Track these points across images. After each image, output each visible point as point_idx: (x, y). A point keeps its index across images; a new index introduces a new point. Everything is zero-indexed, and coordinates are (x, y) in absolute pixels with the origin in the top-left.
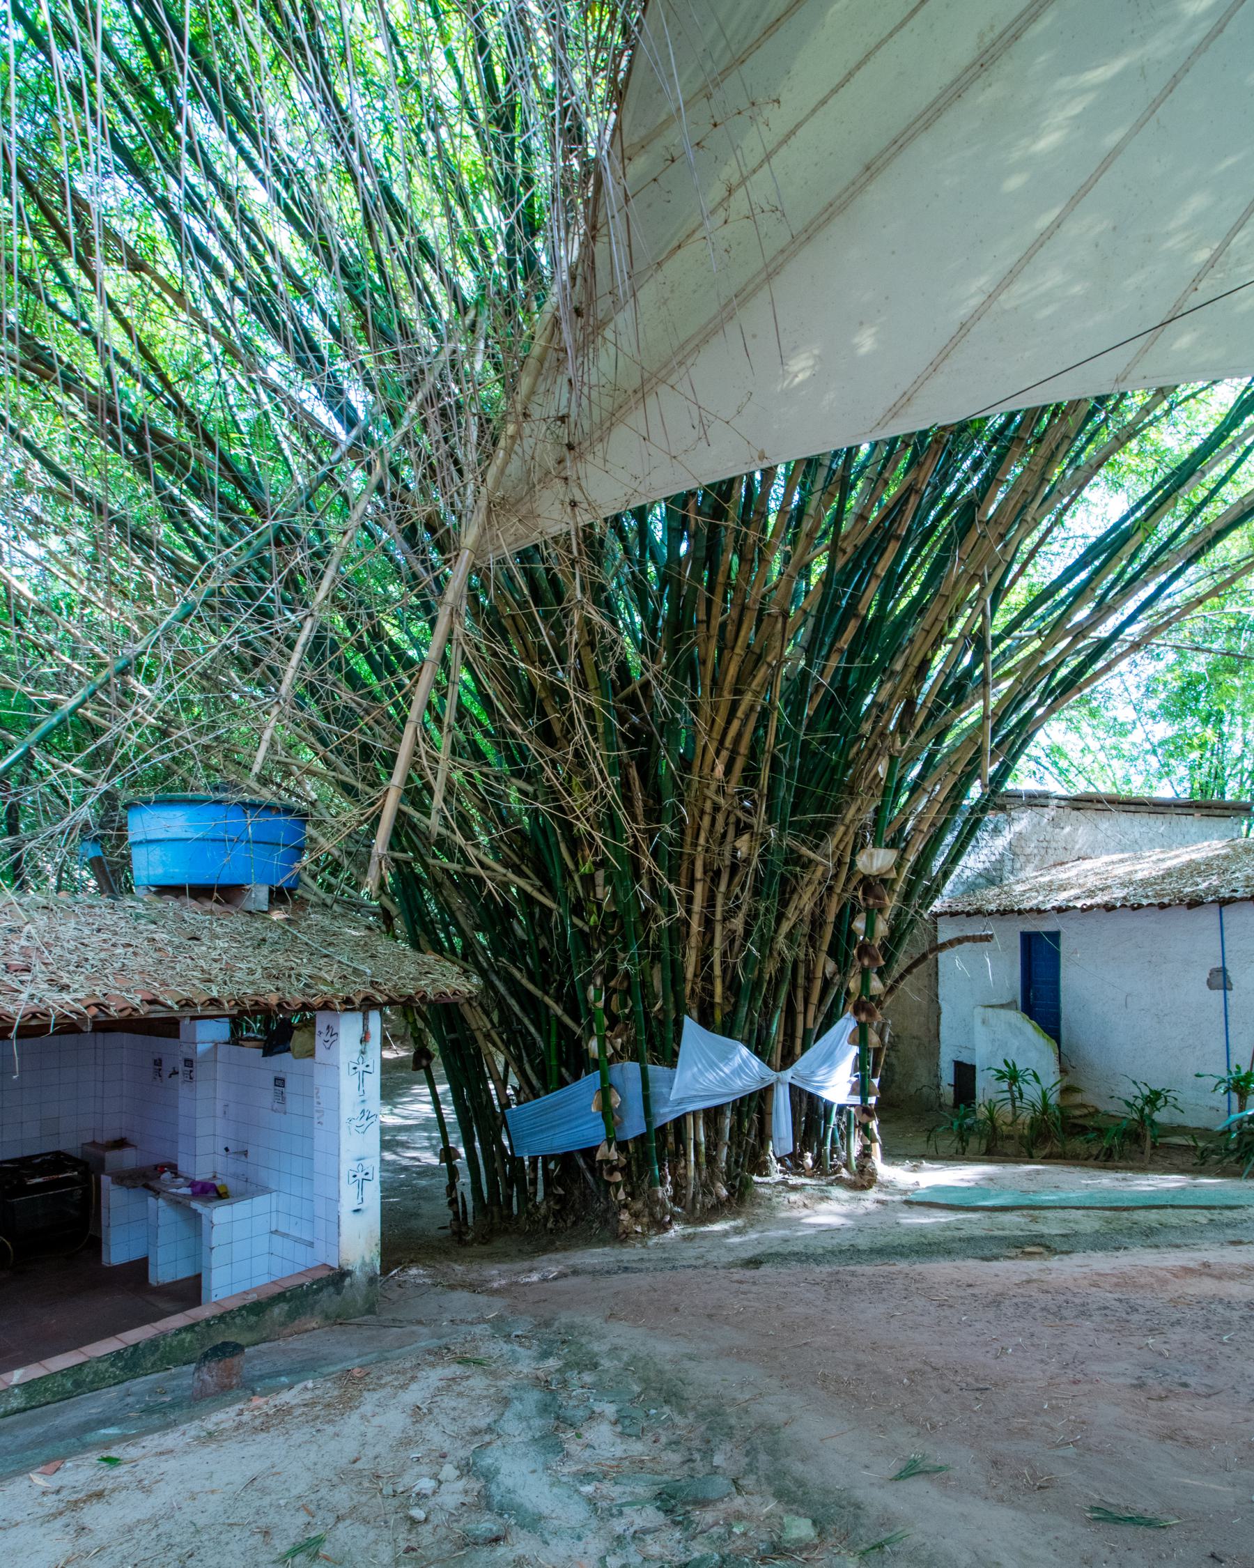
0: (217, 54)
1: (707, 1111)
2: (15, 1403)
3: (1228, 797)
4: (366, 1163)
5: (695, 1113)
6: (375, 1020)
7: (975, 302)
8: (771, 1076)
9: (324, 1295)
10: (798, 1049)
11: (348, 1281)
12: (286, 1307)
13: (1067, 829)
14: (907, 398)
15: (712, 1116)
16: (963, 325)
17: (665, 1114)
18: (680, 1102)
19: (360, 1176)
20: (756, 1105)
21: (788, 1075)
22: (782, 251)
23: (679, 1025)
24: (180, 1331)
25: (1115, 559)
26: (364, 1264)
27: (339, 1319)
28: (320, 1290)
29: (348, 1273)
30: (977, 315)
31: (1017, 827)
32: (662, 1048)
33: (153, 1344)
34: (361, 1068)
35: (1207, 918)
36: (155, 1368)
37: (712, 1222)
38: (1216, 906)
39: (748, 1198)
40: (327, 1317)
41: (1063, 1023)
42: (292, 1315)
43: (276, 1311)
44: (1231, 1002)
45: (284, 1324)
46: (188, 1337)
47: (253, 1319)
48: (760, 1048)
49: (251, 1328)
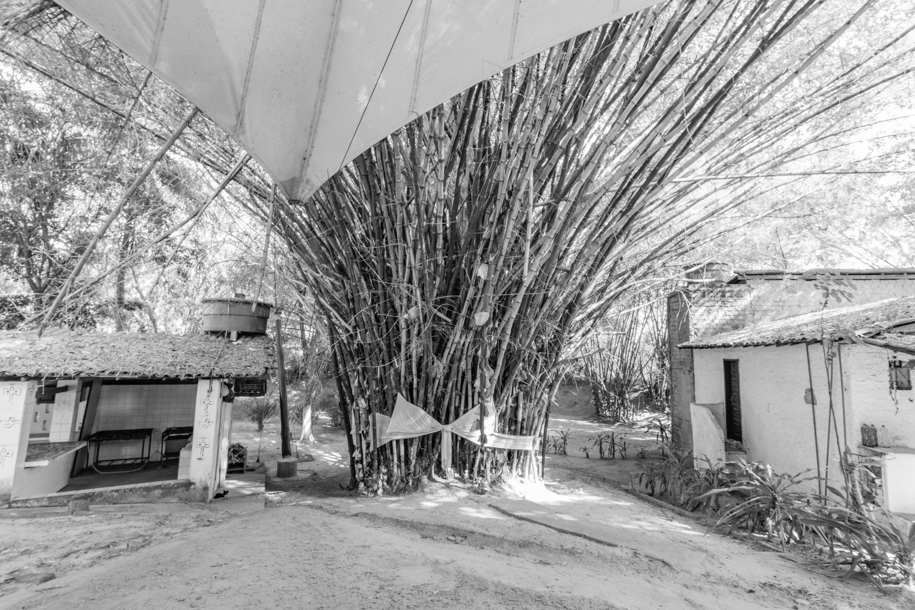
1: (405, 441)
2: (44, 503)
4: (206, 441)
5: (398, 441)
6: (216, 384)
8: (439, 427)
9: (180, 490)
10: (461, 412)
11: (192, 487)
12: (161, 491)
13: (800, 293)
15: (408, 443)
17: (385, 439)
18: (391, 434)
19: (203, 445)
20: (430, 442)
21: (449, 428)
23: (395, 397)
24: (112, 491)
25: (692, 91)
26: (201, 481)
27: (186, 501)
28: (178, 487)
29: (193, 484)
31: (755, 293)
32: (387, 407)
33: (101, 494)
34: (207, 402)
38: (804, 345)
41: (742, 418)
42: (163, 495)
44: (817, 413)
45: (159, 498)
46: (116, 494)
47: (145, 493)
48: (436, 415)
49: (144, 496)
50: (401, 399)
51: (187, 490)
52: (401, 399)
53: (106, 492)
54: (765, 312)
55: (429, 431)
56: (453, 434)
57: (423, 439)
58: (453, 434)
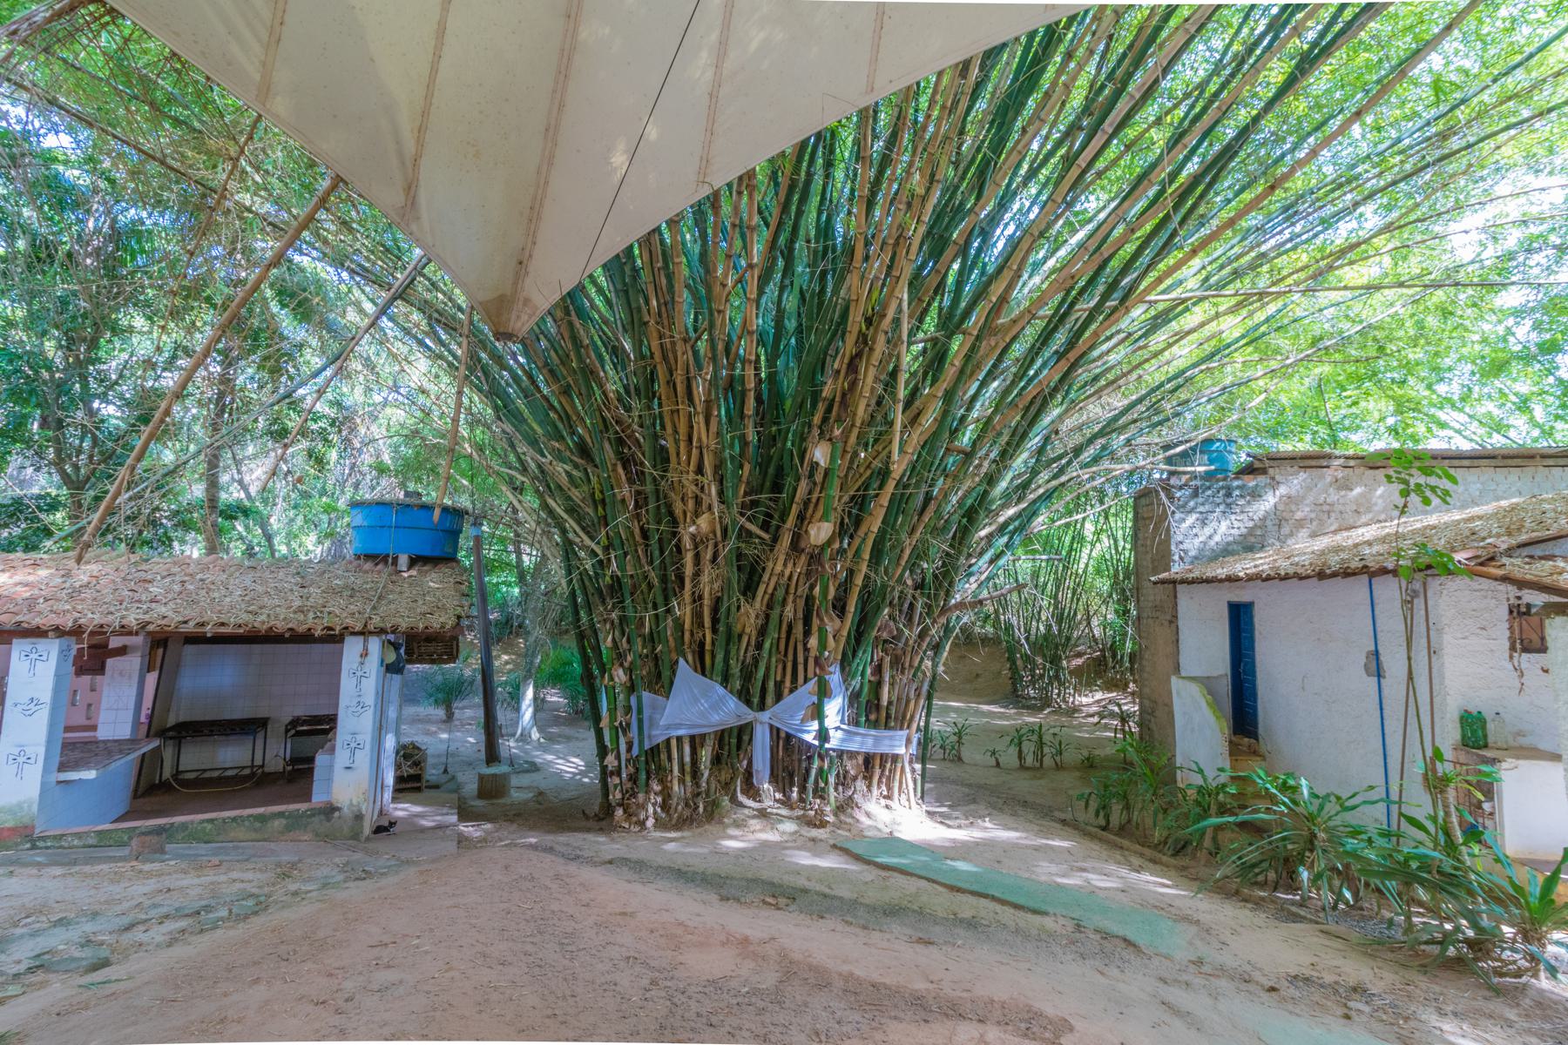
0: (1156, 188)
2: (90, 841)
3: (385, 319)
5: (679, 739)
6: (375, 644)
7: (709, 74)
8: (749, 715)
9: (316, 819)
11: (337, 814)
12: (284, 821)
14: (706, 161)
16: (711, 95)
18: (668, 727)
19: (353, 745)
20: (734, 741)
21: (765, 716)
22: (554, 91)
27: (327, 838)
29: (338, 809)
30: (717, 83)
31: (1282, 490)
32: (660, 680)
33: (184, 826)
35: (1359, 586)
36: (184, 841)
37: (832, 869)
38: (1365, 578)
39: (716, 817)
40: (317, 835)
42: (288, 828)
43: (277, 823)
45: (282, 833)
46: (209, 826)
47: (258, 825)
48: (744, 696)
49: (255, 830)
50: (684, 669)
51: (329, 820)
52: (684, 669)
53: (192, 822)
54: (1300, 524)
55: (733, 722)
56: (771, 726)
57: (722, 736)
58: (771, 726)
